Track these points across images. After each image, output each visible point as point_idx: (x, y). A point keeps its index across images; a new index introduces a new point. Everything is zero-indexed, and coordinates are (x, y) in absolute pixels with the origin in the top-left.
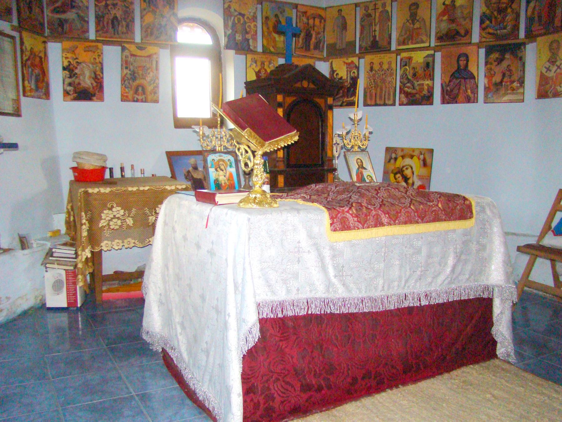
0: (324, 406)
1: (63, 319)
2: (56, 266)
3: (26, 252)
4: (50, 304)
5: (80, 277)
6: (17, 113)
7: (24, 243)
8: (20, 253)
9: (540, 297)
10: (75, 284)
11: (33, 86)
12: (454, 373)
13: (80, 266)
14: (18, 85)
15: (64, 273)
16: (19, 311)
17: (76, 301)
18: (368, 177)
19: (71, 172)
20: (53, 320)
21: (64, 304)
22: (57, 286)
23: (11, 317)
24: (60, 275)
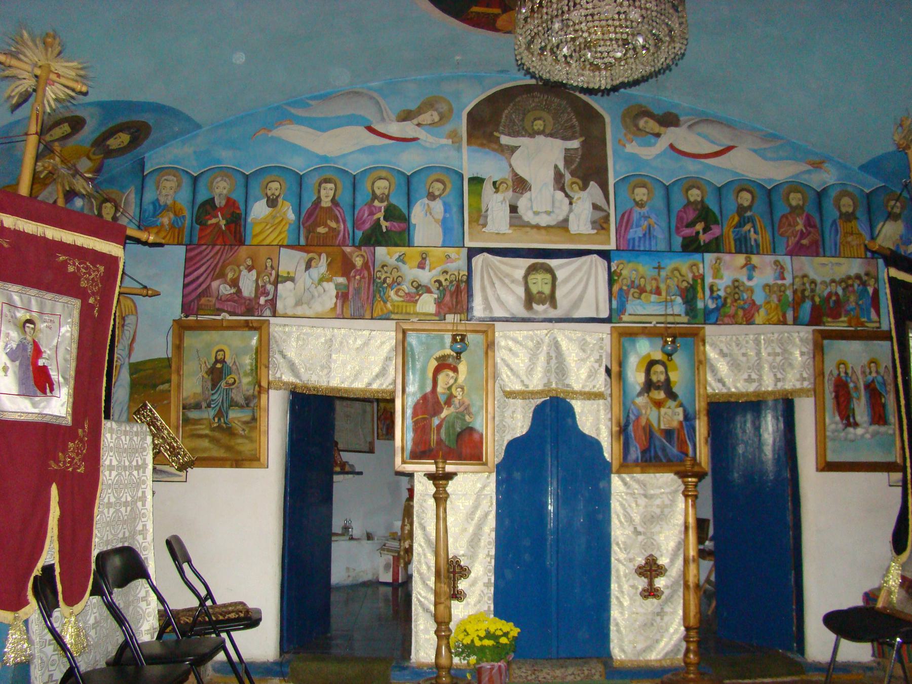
0: (888, 614)
1: (389, 590)
2: (386, 552)
3: (369, 542)
4: (381, 580)
5: (402, 561)
6: (371, 451)
7: (369, 537)
8: (365, 543)
9: (759, 676)
10: (398, 566)
11: (384, 432)
12: (75, 346)
13: (402, 553)
14: (373, 432)
15: (391, 557)
16: (361, 580)
17: (398, 579)
18: (842, 366)
19: (407, 491)
20: (382, 589)
21: (390, 580)
22: (387, 567)
23: (355, 582)
24: (389, 559)
